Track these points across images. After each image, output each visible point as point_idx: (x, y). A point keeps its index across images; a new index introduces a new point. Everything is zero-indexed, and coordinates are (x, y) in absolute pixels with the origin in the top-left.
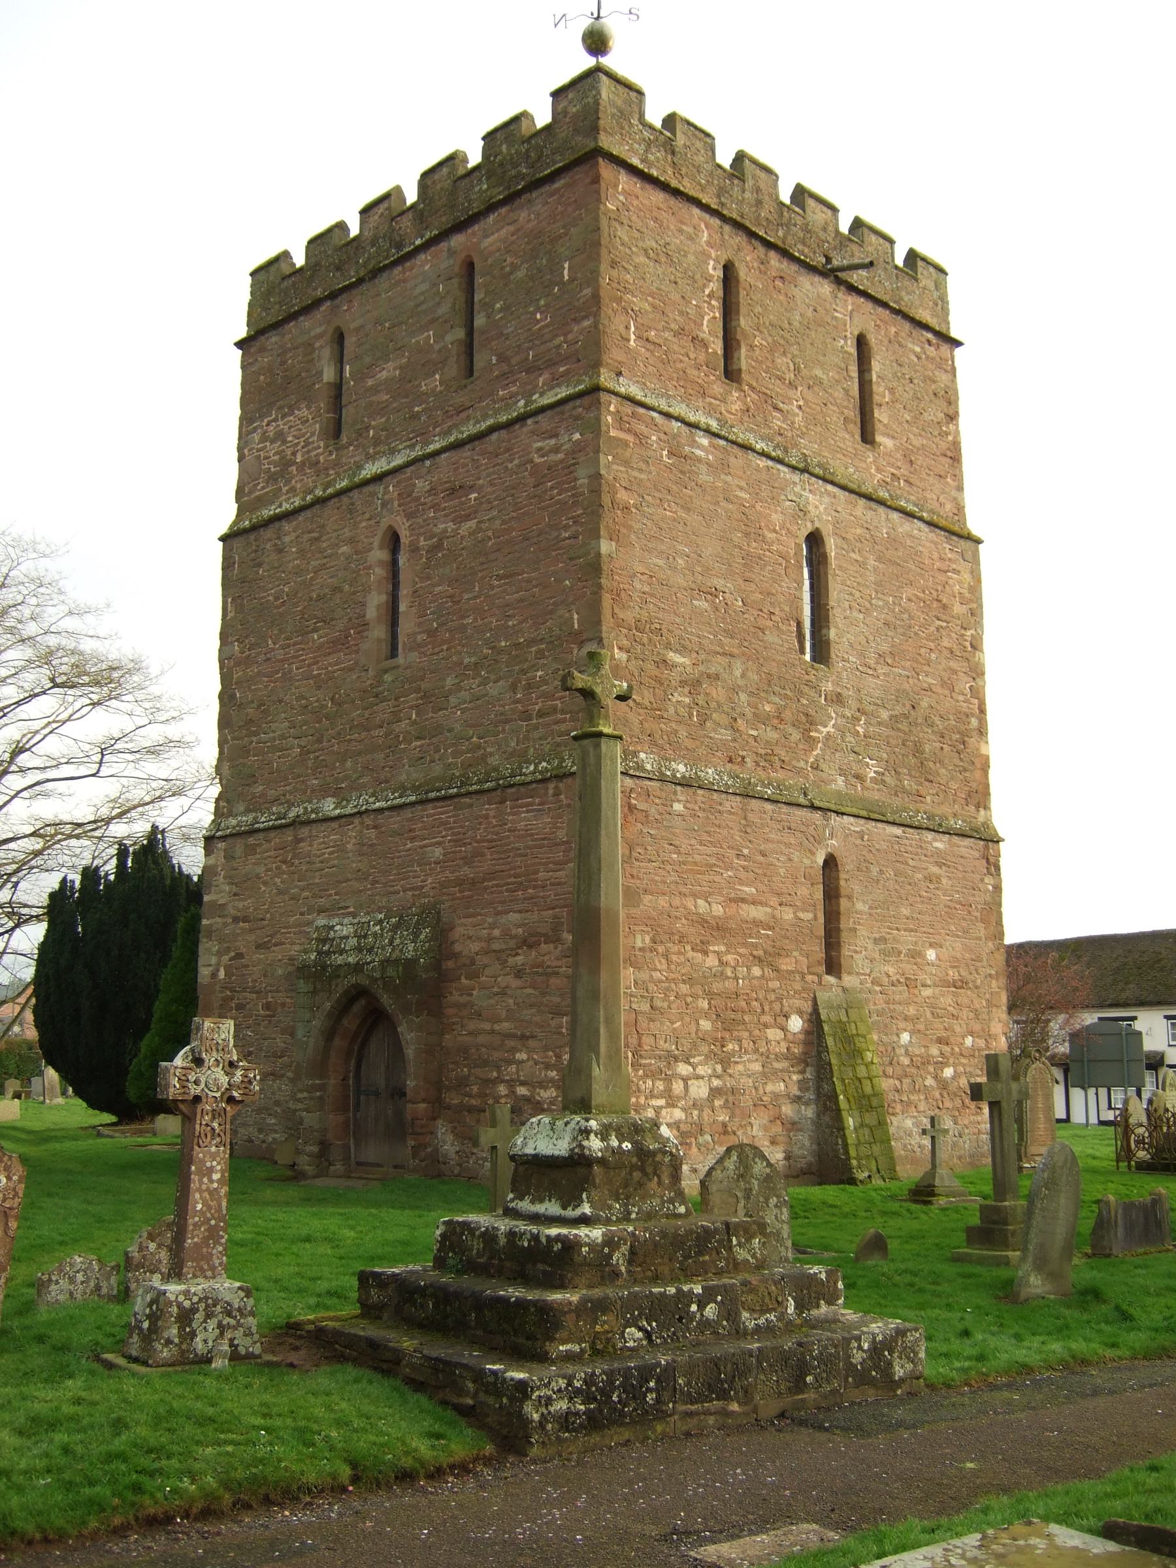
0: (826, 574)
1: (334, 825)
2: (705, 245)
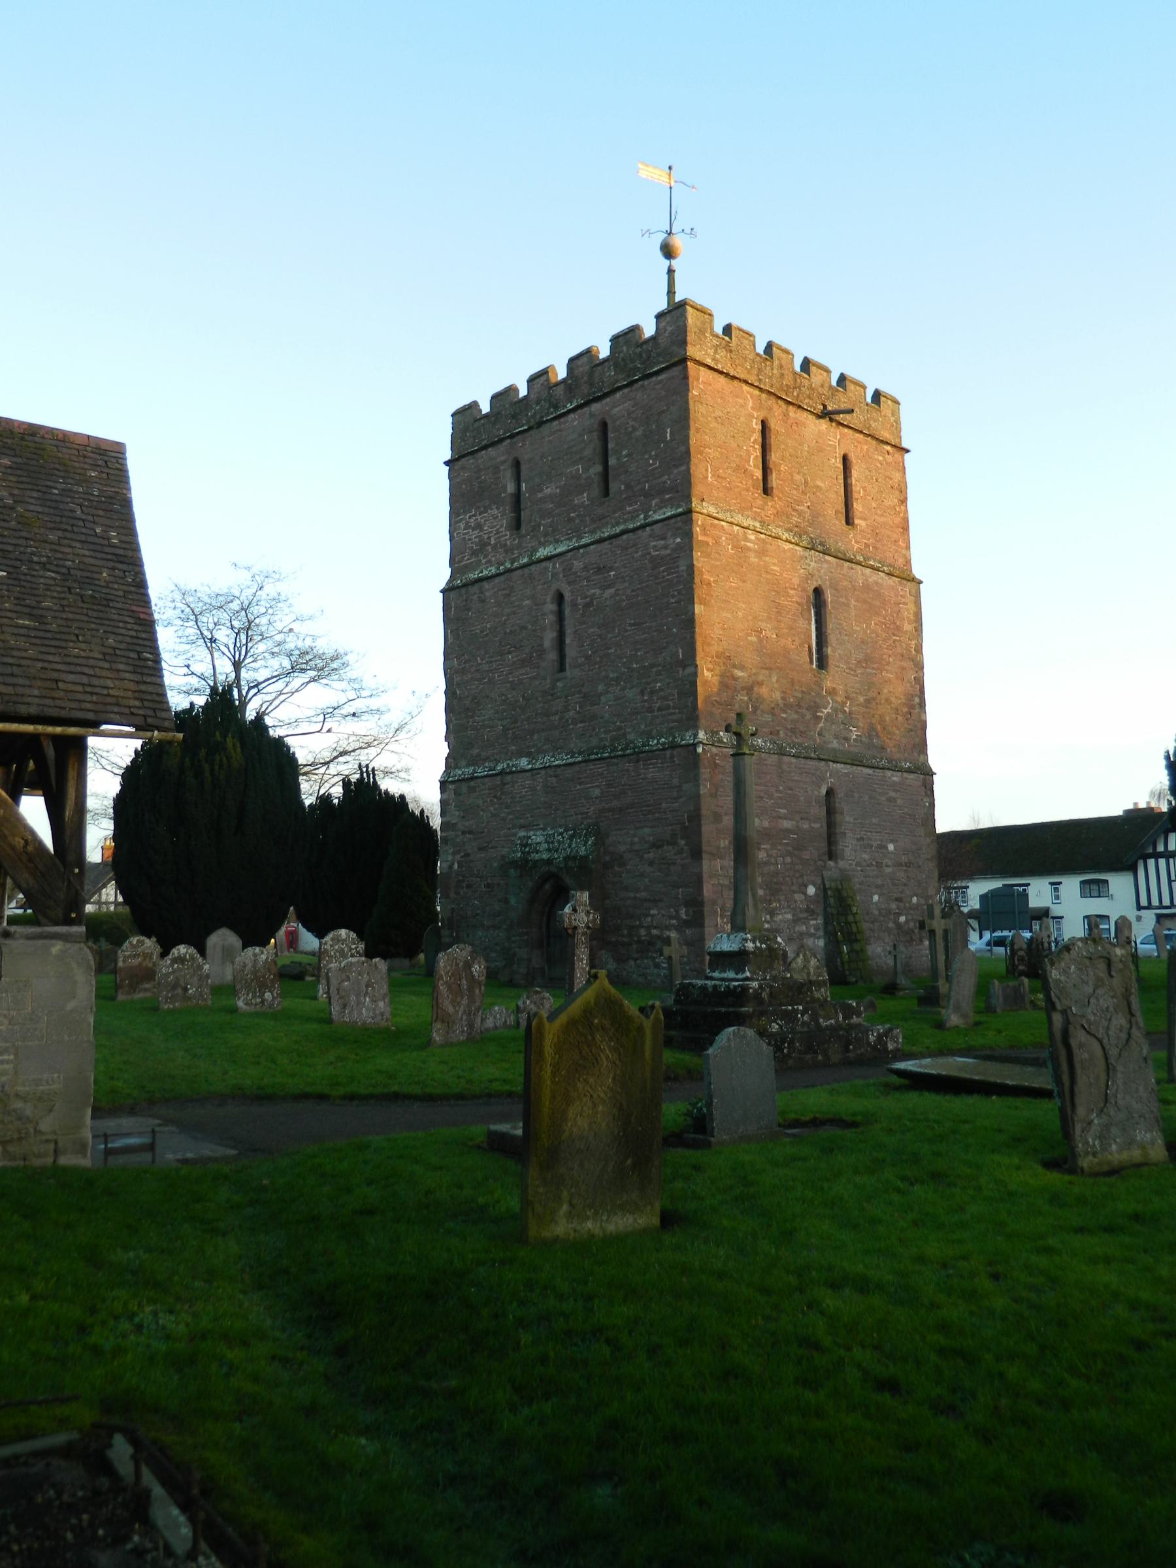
1: (528, 774)
2: (747, 408)
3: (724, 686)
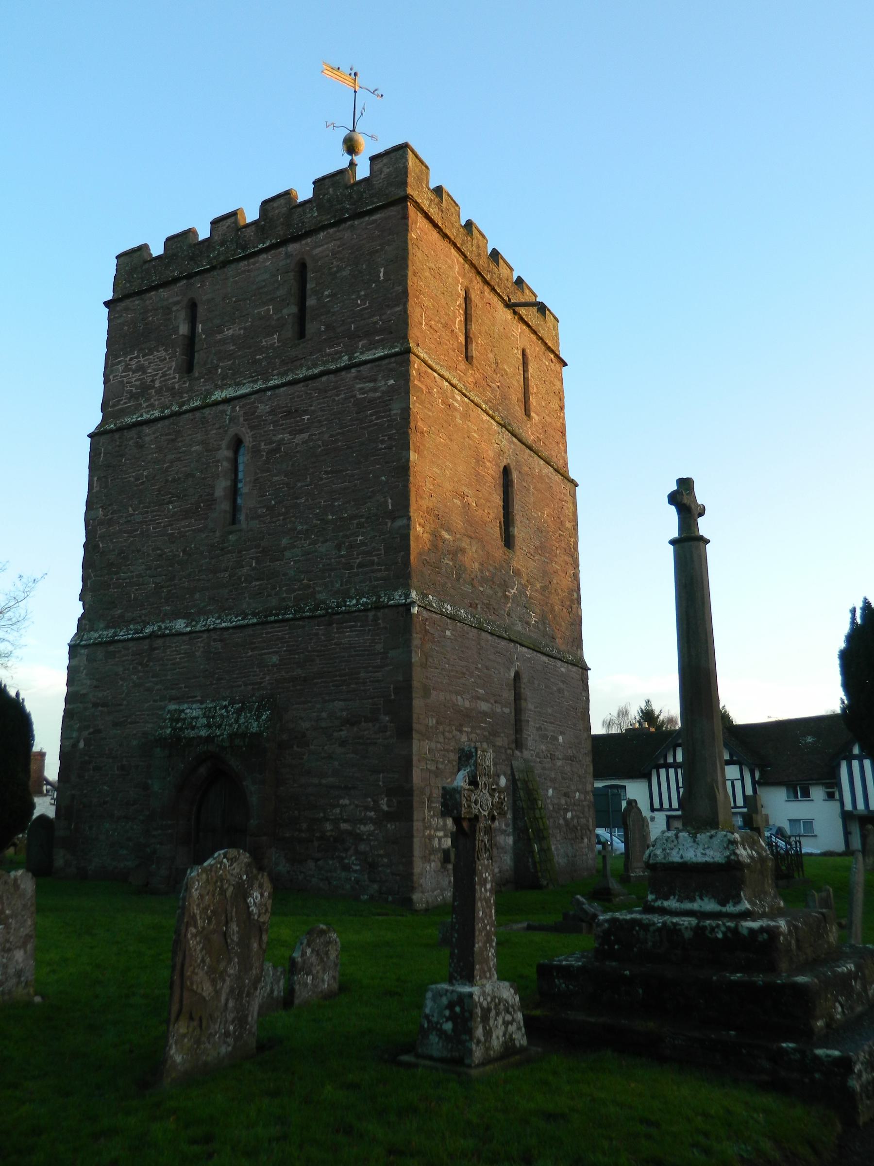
0: (512, 493)
1: (186, 638)
3: (434, 547)
